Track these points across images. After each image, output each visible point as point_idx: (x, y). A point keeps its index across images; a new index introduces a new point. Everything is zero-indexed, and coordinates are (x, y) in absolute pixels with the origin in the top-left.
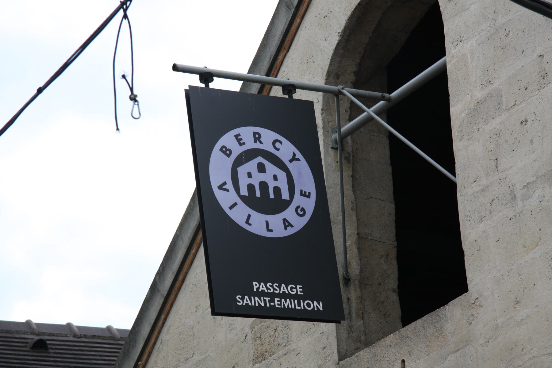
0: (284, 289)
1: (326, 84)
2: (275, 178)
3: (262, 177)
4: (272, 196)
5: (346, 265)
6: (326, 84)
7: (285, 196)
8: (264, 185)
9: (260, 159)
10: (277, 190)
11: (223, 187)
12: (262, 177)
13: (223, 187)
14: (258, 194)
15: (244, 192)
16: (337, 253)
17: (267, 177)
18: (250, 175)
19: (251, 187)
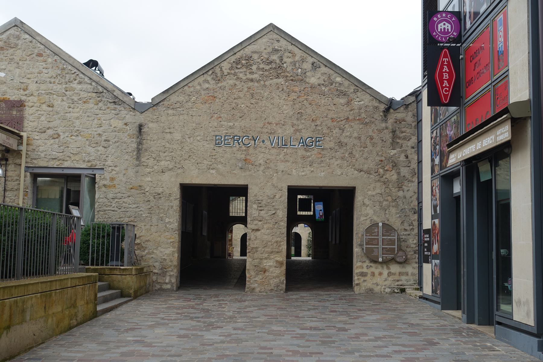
0: (392, 313)
1: (241, 256)
2: (448, 26)
3: (444, 26)
4: (446, 31)
5: (40, 354)
6: (241, 256)
7: (450, 31)
8: (444, 28)
9: (444, 22)
10: (448, 29)
11: (447, 166)
12: (444, 26)
13: (447, 166)
14: (443, 31)
15: (439, 30)
16: (250, 239)
17: (446, 27)
18: (441, 26)
19: (441, 29)
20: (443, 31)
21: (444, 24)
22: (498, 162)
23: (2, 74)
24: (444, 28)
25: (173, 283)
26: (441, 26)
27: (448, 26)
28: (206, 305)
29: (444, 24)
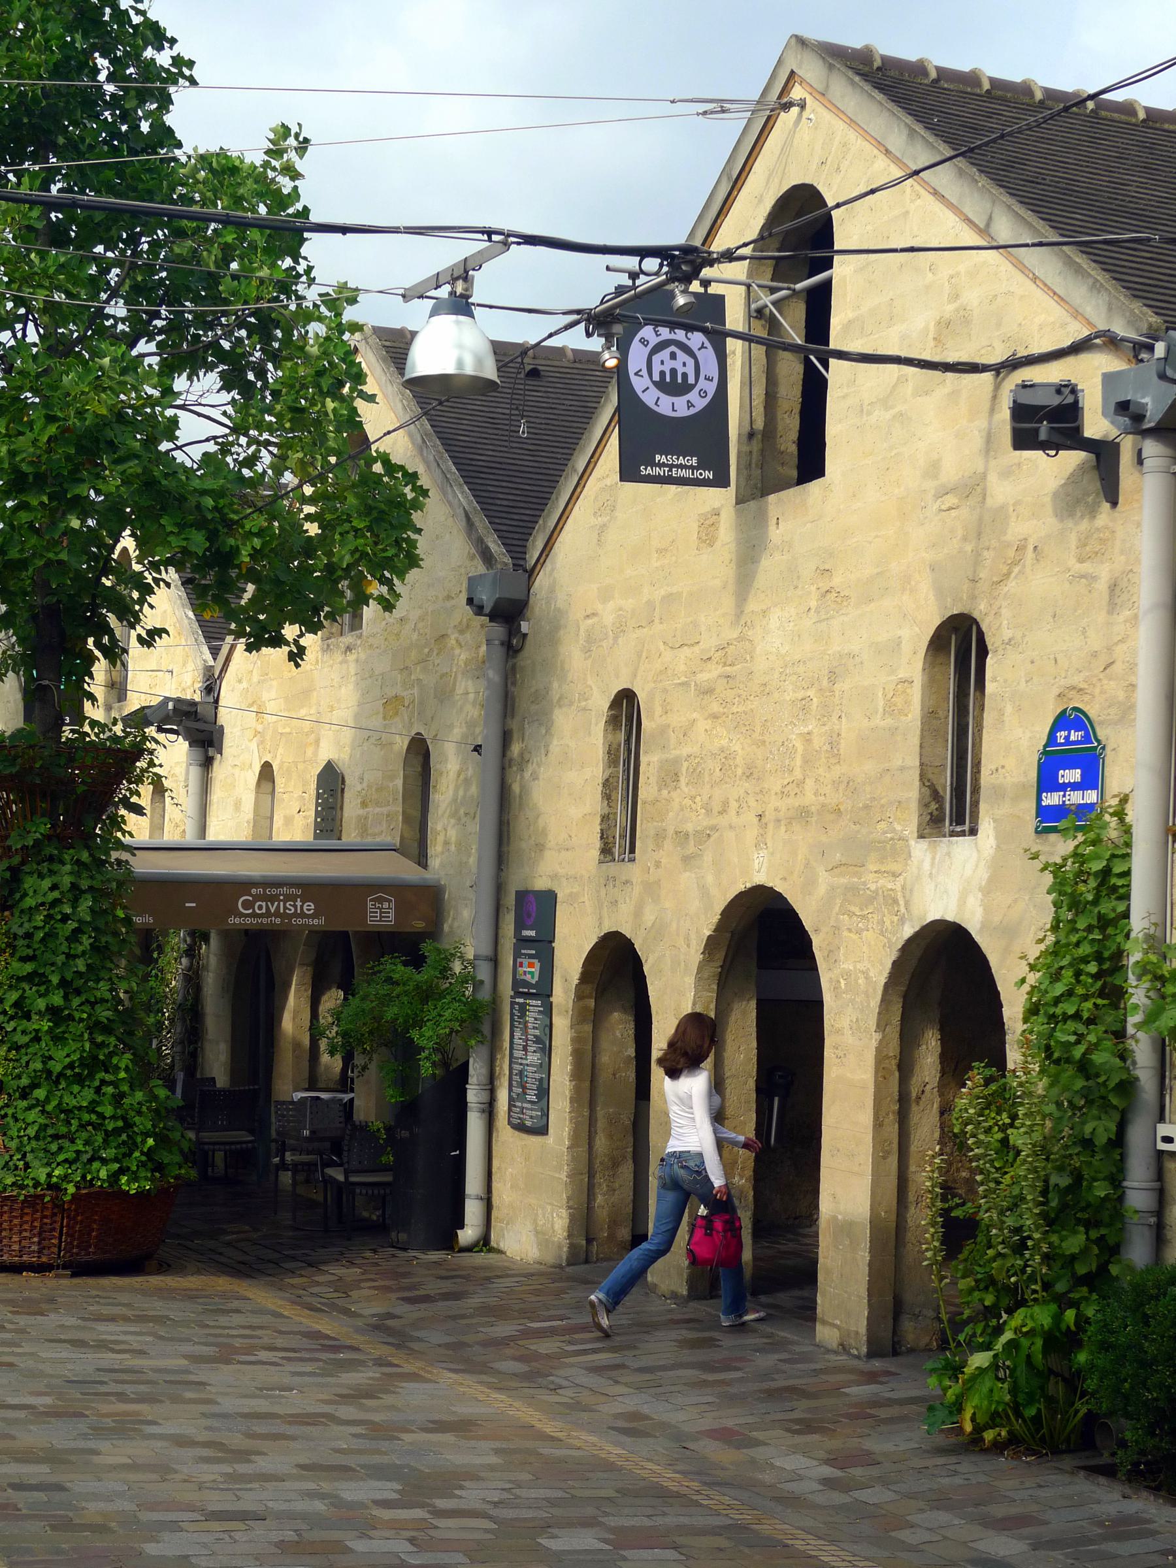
2: (684, 364)
4: (680, 380)
6: (772, 280)
7: (691, 380)
8: (674, 372)
9: (673, 348)
10: (685, 375)
14: (668, 380)
15: (656, 377)
17: (677, 364)
18: (662, 363)
19: (662, 373)
20: (668, 380)
21: (673, 356)
22: (612, 1013)
23: (5, 337)
24: (674, 372)
25: (99, 1179)
26: (662, 363)
27: (684, 364)
28: (439, 827)
29: (673, 356)
